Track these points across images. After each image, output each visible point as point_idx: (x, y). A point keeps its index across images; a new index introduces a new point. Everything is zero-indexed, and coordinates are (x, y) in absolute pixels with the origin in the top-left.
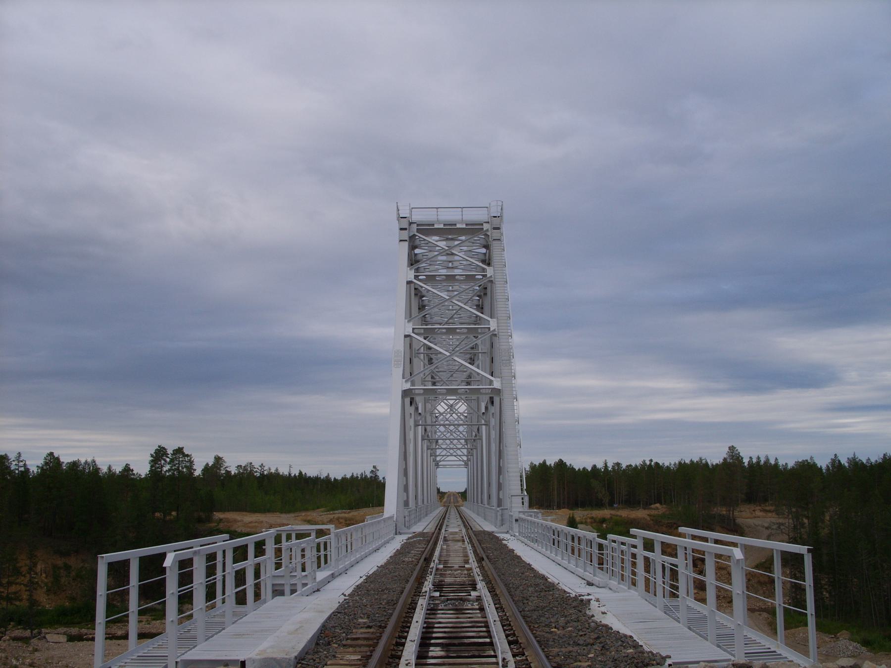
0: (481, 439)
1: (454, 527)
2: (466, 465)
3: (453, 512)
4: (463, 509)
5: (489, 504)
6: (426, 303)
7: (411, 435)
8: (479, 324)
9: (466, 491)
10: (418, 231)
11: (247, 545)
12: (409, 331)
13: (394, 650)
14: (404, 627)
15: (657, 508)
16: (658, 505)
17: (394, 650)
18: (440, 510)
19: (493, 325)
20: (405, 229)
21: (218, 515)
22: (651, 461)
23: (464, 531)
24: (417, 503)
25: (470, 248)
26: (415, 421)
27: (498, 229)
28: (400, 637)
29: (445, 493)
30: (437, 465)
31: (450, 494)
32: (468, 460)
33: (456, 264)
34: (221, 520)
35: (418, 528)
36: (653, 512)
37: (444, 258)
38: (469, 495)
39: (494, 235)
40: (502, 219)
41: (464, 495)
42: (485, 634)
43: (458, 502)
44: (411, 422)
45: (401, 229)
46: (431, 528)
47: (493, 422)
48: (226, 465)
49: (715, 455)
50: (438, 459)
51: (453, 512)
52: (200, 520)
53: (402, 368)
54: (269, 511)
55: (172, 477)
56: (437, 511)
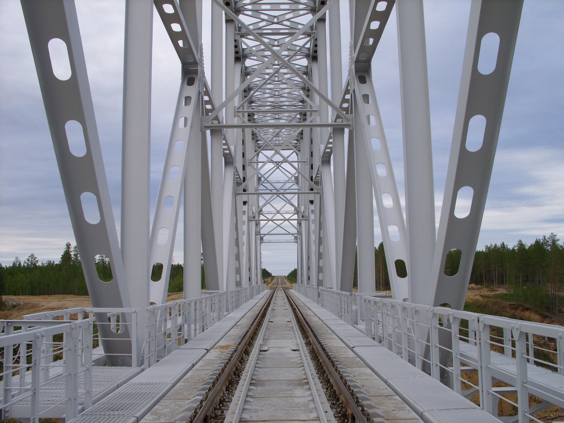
3: (280, 296)
4: (293, 292)
18: (267, 292)
31: (278, 277)
33: (281, 92)
37: (272, 99)
38: (302, 276)
41: (293, 276)
43: (285, 283)
51: (280, 296)
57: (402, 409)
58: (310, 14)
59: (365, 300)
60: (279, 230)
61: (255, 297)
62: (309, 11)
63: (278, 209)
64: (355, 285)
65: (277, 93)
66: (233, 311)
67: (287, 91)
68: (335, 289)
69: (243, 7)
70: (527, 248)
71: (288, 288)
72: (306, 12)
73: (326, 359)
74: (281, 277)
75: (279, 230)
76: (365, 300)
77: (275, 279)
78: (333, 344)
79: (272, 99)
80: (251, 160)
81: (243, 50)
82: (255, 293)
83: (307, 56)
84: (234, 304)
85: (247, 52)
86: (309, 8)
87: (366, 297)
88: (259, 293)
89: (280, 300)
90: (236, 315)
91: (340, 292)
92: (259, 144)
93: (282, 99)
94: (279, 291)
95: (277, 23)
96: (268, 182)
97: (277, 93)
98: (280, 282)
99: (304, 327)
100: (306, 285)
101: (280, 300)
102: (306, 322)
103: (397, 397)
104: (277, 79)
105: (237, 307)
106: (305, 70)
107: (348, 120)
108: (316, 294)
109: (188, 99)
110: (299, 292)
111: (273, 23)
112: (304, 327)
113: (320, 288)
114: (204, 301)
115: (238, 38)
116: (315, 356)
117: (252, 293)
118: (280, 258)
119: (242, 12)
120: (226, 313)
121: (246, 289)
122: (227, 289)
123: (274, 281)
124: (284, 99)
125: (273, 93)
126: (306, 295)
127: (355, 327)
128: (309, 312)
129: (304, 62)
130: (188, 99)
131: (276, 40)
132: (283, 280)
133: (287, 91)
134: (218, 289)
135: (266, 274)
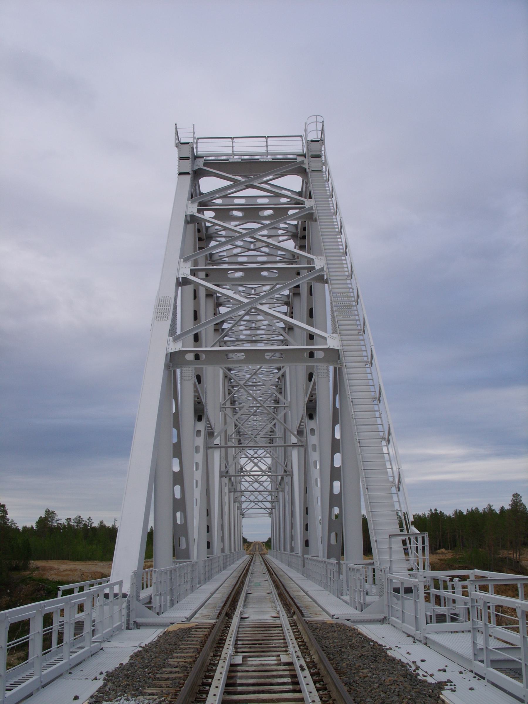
0: (291, 475)
1: (261, 610)
2: (271, 514)
3: (258, 561)
4: (268, 557)
5: (284, 550)
6: (236, 399)
7: (226, 499)
8: (296, 263)
9: (270, 540)
10: (205, 165)
11: (74, 589)
12: (185, 271)
13: (224, 630)
14: (204, 684)
15: (443, 553)
16: (443, 550)
17: (222, 636)
18: (246, 557)
19: (319, 263)
20: (187, 158)
21: (34, 563)
22: (436, 510)
23: (285, 620)
24: (230, 550)
25: (269, 370)
26: (229, 489)
27: (319, 156)
28: (206, 677)
29: (251, 543)
30: (243, 515)
31: (256, 544)
32: (273, 508)
33: (259, 324)
34: (38, 568)
35: (179, 615)
36: (442, 557)
37: (248, 332)
38: (274, 543)
39: (313, 164)
40: (323, 143)
41: (268, 544)
42: (289, 680)
43: (262, 550)
44: (226, 490)
45: (181, 158)
46: (206, 617)
47: (287, 488)
48: (57, 518)
49: (501, 502)
50: (244, 506)
51: (258, 561)
52: (16, 569)
53: (169, 322)
54: (90, 559)
55: (9, 527)
56: (241, 561)
57: (300, 592)
58: (292, 240)
59: (350, 569)
60: (256, 506)
61: (229, 568)
62: (290, 237)
63: (256, 488)
64: (343, 554)
65: (253, 325)
66: (205, 583)
67: (266, 322)
68: (320, 558)
69: (216, 233)
70: (498, 512)
71: (264, 554)
72: (286, 237)
73: (280, 584)
74: (259, 543)
75: (256, 506)
76: (350, 569)
77: (252, 545)
78: (292, 587)
79: (248, 332)
80: (231, 436)
81: (207, 228)
82: (228, 563)
83: (294, 236)
84: (207, 576)
85: (212, 231)
86: (291, 234)
87: (351, 565)
88: (233, 563)
89: (258, 567)
90: (209, 587)
91: (326, 560)
92: (231, 382)
93: (259, 332)
94: (257, 557)
95: (254, 250)
96: (248, 482)
97: (253, 325)
98: (257, 549)
99: (271, 572)
100: (289, 553)
101: (258, 567)
102: (281, 582)
103: (324, 613)
104: (254, 380)
105: (210, 578)
106: (286, 300)
107: (302, 442)
108: (300, 563)
109: (199, 432)
110: (277, 558)
111: (250, 250)
112: (271, 572)
113: (306, 556)
114: (178, 570)
115: (230, 388)
116: (274, 581)
117: (226, 563)
118: (257, 527)
119: (214, 239)
120: (198, 586)
121: (219, 557)
122: (197, 558)
123: (251, 548)
124: (262, 332)
125: (249, 325)
126: (290, 565)
127: (339, 598)
128: (282, 573)
129: (290, 245)
130: (199, 432)
131: (252, 288)
132: (261, 546)
133: (266, 322)
134: (189, 558)
135: (245, 541)
